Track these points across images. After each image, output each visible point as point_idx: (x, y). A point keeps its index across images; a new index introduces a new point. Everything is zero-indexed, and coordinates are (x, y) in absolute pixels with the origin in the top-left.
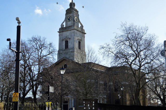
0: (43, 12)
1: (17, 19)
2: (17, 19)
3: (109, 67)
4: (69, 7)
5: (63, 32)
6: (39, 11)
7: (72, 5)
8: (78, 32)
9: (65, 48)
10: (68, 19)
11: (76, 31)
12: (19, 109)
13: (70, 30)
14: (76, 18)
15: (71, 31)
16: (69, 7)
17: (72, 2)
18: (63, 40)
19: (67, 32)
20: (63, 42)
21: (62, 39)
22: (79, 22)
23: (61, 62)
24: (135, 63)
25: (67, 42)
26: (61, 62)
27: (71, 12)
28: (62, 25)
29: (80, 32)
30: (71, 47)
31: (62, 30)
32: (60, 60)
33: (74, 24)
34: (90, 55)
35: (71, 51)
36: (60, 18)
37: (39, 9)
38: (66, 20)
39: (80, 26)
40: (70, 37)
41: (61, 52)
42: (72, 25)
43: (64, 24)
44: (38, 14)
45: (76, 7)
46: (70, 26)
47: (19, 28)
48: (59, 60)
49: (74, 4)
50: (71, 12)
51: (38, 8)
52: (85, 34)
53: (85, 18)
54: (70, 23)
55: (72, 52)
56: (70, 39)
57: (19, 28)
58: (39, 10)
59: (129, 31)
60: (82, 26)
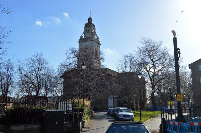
0: (42, 23)
1: (174, 32)
2: (174, 32)
3: (120, 72)
4: (87, 22)
6: (39, 23)
7: (90, 20)
8: (95, 43)
10: (86, 32)
11: (94, 42)
14: (93, 31)
16: (87, 22)
17: (90, 17)
22: (96, 34)
27: (89, 26)
28: (82, 36)
29: (97, 42)
31: (81, 40)
33: (92, 36)
36: (80, 31)
37: (39, 21)
38: (84, 33)
39: (96, 37)
42: (91, 36)
43: (83, 35)
44: (38, 25)
45: (93, 22)
46: (88, 37)
47: (175, 40)
49: (92, 19)
50: (89, 26)
51: (38, 20)
52: (100, 44)
53: (99, 32)
54: (88, 35)
57: (175, 40)
58: (39, 21)
59: (148, 43)
60: (98, 38)
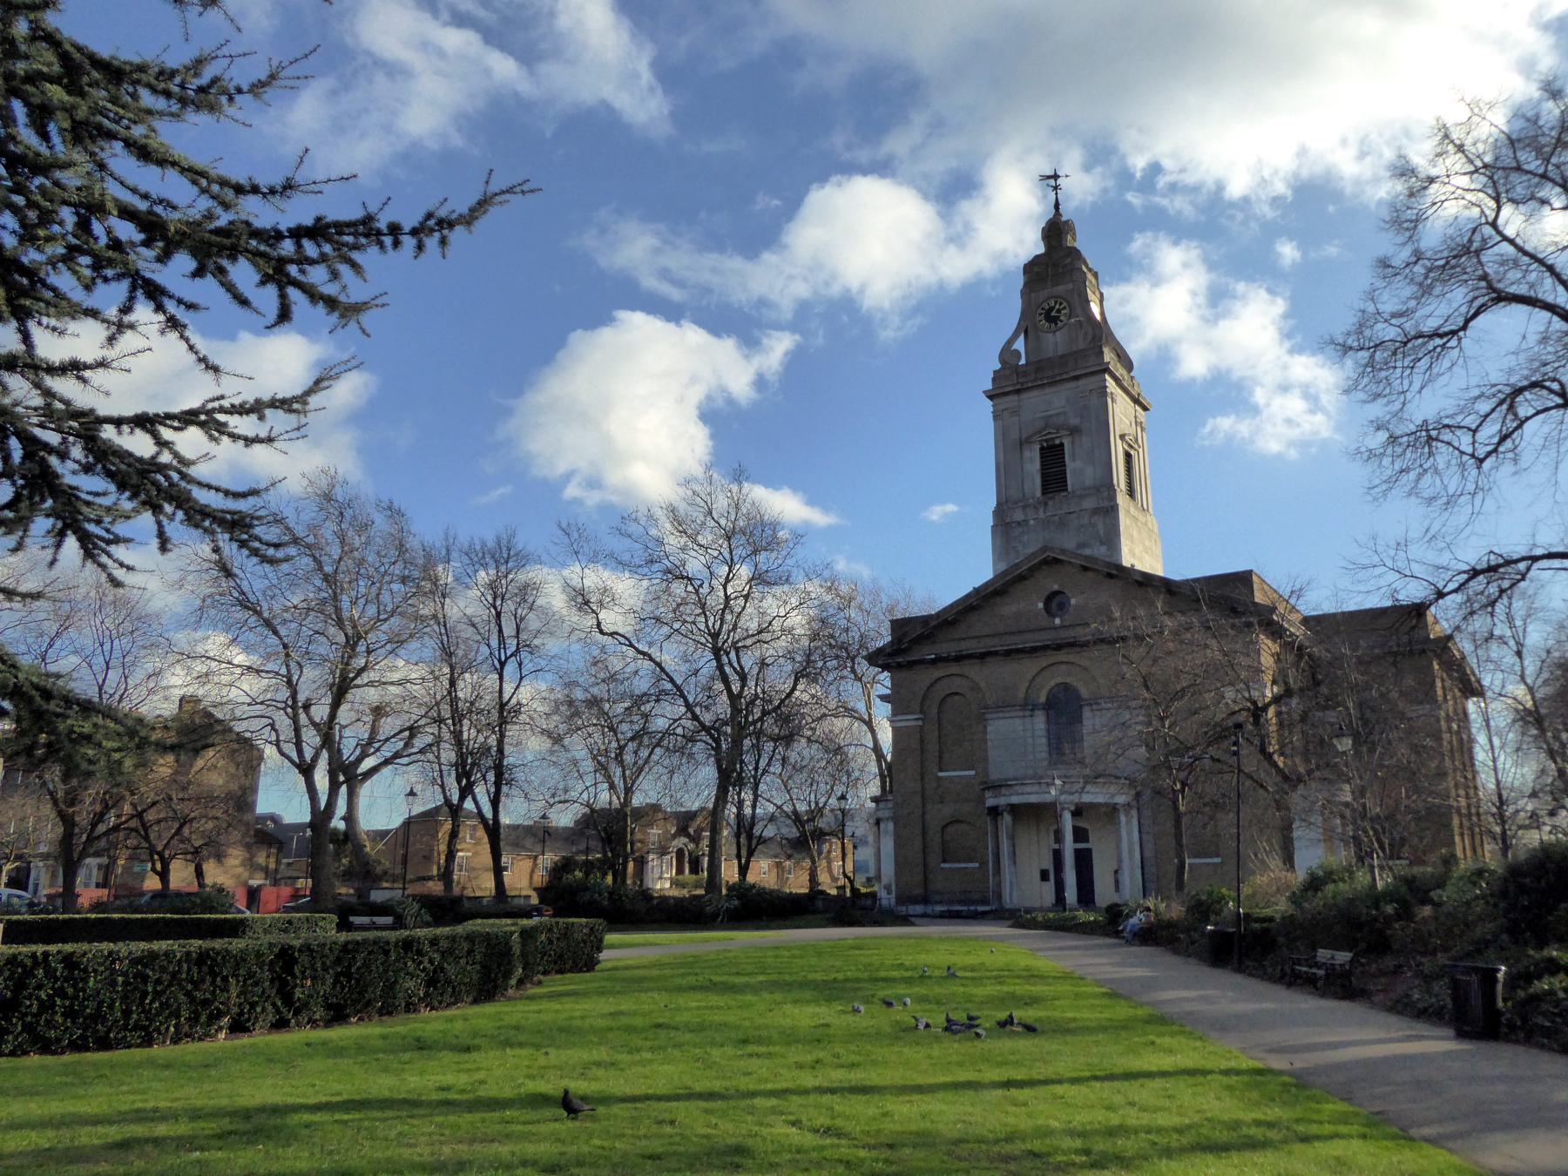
5: (1025, 396)
9: (1046, 489)
12: (13, 961)
13: (1076, 378)
15: (1081, 382)
18: (1023, 443)
19: (1048, 390)
20: (1027, 454)
21: (1015, 435)
23: (1021, 578)
24: (853, 671)
25: (1053, 458)
26: (1021, 578)
28: (1007, 354)
30: (1088, 483)
32: (1005, 573)
34: (509, 630)
35: (1089, 504)
38: (1026, 327)
40: (1074, 421)
41: (1019, 515)
43: (1020, 345)
48: (1003, 567)
54: (1055, 342)
55: (1096, 511)
56: (1074, 431)
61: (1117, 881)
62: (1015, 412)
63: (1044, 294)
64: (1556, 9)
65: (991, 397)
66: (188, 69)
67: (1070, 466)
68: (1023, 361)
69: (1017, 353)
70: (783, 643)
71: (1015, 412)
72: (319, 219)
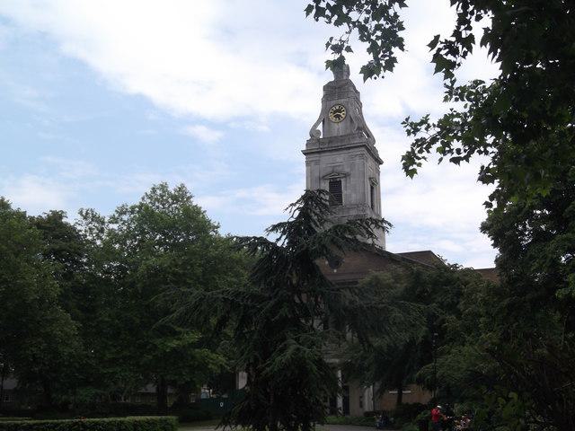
21: (317, 175)
28: (314, 133)
38: (324, 119)
43: (320, 128)
54: (339, 128)
56: (346, 175)
61: (361, 402)
62: (317, 163)
63: (334, 102)
64: (449, 3)
65: (305, 154)
66: (565, 173)
67: (344, 192)
68: (321, 137)
69: (543, 214)
70: (415, 368)
71: (317, 163)
72: (484, 228)
